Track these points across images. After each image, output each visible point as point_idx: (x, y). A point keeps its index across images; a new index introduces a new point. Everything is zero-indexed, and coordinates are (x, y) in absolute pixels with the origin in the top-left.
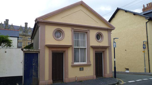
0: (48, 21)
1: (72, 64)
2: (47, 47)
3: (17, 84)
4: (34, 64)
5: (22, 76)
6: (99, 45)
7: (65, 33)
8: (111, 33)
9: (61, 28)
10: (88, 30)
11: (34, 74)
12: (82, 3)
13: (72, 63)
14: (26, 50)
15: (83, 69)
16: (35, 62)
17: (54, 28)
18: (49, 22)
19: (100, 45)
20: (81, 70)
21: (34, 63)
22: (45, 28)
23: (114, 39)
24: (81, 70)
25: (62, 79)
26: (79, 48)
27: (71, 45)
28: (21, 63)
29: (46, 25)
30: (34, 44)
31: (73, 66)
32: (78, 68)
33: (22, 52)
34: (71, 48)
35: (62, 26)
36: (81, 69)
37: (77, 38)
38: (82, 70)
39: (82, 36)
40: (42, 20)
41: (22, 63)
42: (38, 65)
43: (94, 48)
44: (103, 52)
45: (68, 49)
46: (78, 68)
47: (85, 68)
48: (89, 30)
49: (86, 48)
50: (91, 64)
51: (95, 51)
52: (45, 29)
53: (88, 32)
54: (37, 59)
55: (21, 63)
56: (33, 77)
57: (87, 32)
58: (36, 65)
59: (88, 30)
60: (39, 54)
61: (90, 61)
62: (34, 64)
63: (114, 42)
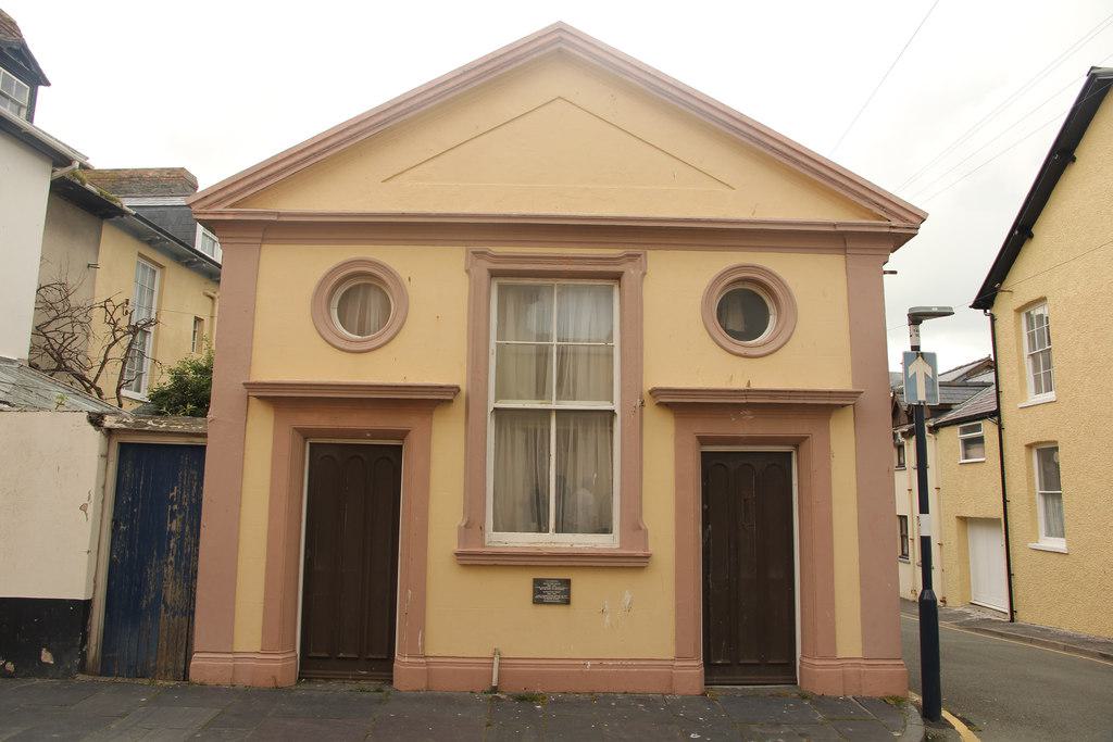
0: (273, 214)
2: (660, 404)
3: (44, 651)
4: (174, 526)
5: (85, 606)
6: (740, 385)
7: (412, 289)
8: (886, 268)
10: (632, 251)
11: (172, 592)
13: (472, 527)
14: (117, 426)
15: (568, 592)
17: (323, 260)
18: (279, 214)
19: (754, 386)
20: (547, 598)
21: (173, 516)
23: (916, 318)
24: (547, 598)
25: (781, 664)
26: (549, 411)
27: (845, 384)
28: (84, 508)
29: (264, 240)
30: (1033, 390)
31: (475, 561)
32: (522, 584)
33: (94, 438)
35: (760, 248)
36: (552, 589)
38: (557, 598)
40: (232, 206)
41: (90, 510)
42: (199, 528)
43: (683, 406)
44: (797, 442)
45: (829, 417)
46: (522, 584)
47: (582, 585)
48: (632, 257)
49: (616, 406)
50: (647, 557)
51: (703, 440)
53: (630, 271)
54: (198, 487)
55: (84, 508)
57: (617, 277)
58: (191, 529)
59: (632, 251)
60: (794, 455)
63: (916, 348)
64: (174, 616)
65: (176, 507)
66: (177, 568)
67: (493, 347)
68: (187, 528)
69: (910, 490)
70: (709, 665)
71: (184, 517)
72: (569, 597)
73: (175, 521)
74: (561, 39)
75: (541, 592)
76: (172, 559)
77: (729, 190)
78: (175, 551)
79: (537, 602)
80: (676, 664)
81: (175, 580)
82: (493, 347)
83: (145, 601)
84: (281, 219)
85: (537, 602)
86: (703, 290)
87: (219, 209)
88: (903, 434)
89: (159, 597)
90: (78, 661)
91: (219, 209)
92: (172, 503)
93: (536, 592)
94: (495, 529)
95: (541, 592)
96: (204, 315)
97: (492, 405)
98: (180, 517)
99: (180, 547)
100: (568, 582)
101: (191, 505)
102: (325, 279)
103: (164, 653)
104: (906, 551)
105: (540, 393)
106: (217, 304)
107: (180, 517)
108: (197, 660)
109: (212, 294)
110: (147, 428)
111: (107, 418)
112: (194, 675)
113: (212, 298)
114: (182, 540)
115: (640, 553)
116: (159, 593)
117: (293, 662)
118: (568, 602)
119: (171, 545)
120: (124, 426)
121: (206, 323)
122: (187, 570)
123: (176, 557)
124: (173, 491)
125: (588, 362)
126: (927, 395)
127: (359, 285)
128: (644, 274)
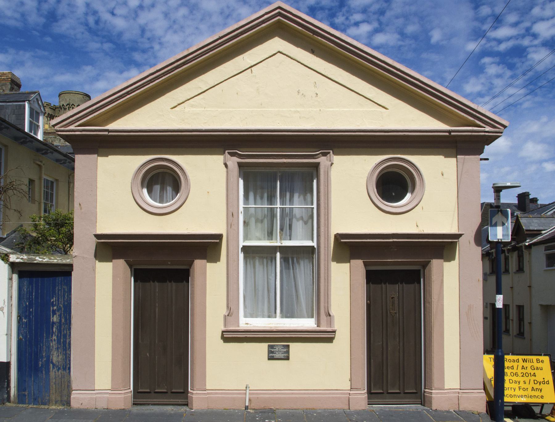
1: (225, 325)
4: (55, 319)
5: (238, 326)
9: (241, 159)
11: (56, 357)
12: (279, 14)
14: (18, 260)
15: (288, 352)
16: (59, 309)
21: (54, 313)
22: (497, 228)
24: (277, 356)
34: (51, 126)
37: (288, 211)
38: (282, 356)
39: (302, 197)
47: (294, 347)
48: (325, 154)
52: (74, 171)
56: (53, 373)
58: (66, 320)
61: (330, 315)
62: (55, 319)
64: (58, 370)
65: (55, 308)
66: (59, 342)
67: (241, 209)
68: (63, 320)
69: (530, 287)
70: (370, 393)
71: (61, 314)
72: (289, 354)
73: (55, 316)
74: (279, 14)
75: (272, 352)
76: (54, 337)
77: (384, 110)
78: (56, 334)
79: (270, 358)
80: (351, 392)
81: (58, 350)
82: (241, 209)
83: (40, 362)
84: (110, 134)
85: (270, 358)
86: (368, 173)
87: (72, 127)
88: (508, 250)
89: (49, 361)
90: (6, 396)
91: (72, 127)
92: (53, 306)
93: (270, 352)
94: (245, 316)
95: (272, 352)
96: (35, 177)
97: (242, 243)
98: (58, 313)
99: (60, 331)
100: (288, 346)
101: (64, 306)
102: (140, 169)
103: (54, 392)
104: (508, 327)
105: (270, 235)
106: (43, 169)
107: (58, 313)
108: (74, 395)
109: (40, 163)
110: (35, 262)
111: (11, 256)
112: (75, 404)
113: (39, 165)
114: (60, 326)
115: (329, 329)
116: (48, 357)
117: (130, 394)
118: (287, 358)
119: (54, 330)
120: (22, 261)
121: (37, 183)
122: (65, 342)
123: (57, 337)
124: (53, 298)
125: (304, 264)
126: (503, 235)
127: (159, 173)
128: (332, 164)
